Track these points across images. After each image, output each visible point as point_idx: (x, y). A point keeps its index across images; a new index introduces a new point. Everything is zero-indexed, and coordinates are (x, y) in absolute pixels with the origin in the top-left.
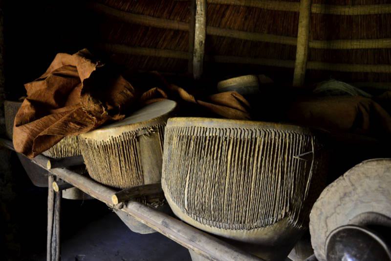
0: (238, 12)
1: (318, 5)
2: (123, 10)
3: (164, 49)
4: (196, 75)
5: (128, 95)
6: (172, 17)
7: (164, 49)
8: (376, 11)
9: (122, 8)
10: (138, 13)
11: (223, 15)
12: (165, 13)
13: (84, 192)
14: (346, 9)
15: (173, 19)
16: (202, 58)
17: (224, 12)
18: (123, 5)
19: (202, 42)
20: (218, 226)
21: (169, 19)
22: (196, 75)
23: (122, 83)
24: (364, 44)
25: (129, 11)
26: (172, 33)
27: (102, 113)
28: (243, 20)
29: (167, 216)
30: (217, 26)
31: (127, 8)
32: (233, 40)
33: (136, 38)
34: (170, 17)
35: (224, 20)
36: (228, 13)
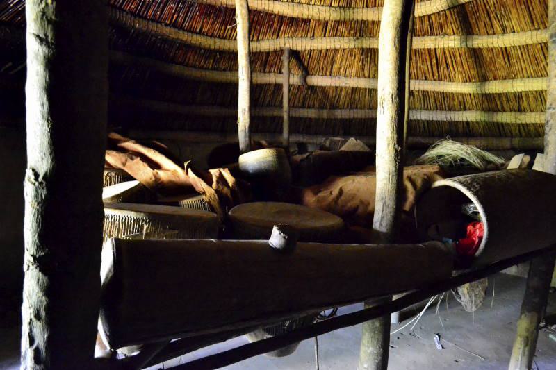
0: (351, 55)
2: (207, 69)
4: (119, 145)
5: (123, 20)
6: (267, 70)
9: (205, 66)
10: (225, 70)
11: (333, 61)
13: (246, 202)
14: (494, 40)
15: (270, 72)
18: (205, 63)
21: (264, 72)
22: (119, 145)
23: (393, 299)
24: (530, 84)
25: (214, 69)
27: (223, 21)
28: (361, 64)
29: (256, 170)
31: (211, 66)
32: (354, 90)
34: (265, 69)
35: (336, 66)
36: (338, 59)
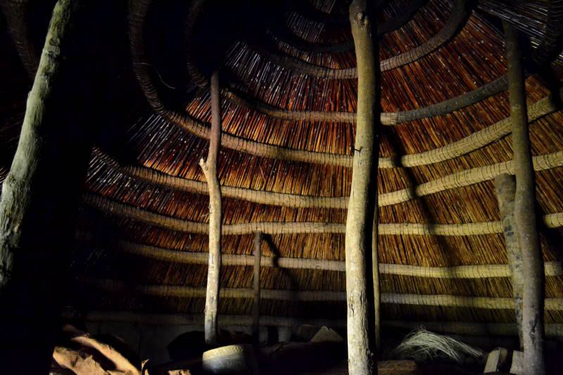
0: (321, 239)
1: (419, 225)
3: (238, 287)
6: (239, 252)
7: (238, 287)
8: (269, 296)
11: (304, 244)
12: (229, 248)
16: (214, 316)
17: (303, 241)
19: (213, 298)
20: (507, 295)
21: (236, 254)
25: (184, 250)
26: (243, 269)
30: (299, 256)
31: (182, 247)
32: (325, 272)
33: (491, 211)
35: (307, 249)
36: (309, 242)
